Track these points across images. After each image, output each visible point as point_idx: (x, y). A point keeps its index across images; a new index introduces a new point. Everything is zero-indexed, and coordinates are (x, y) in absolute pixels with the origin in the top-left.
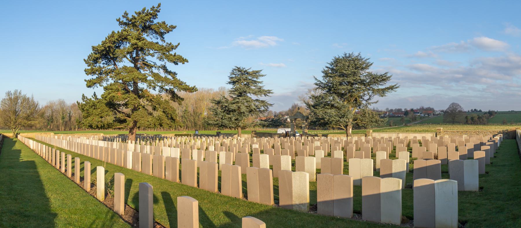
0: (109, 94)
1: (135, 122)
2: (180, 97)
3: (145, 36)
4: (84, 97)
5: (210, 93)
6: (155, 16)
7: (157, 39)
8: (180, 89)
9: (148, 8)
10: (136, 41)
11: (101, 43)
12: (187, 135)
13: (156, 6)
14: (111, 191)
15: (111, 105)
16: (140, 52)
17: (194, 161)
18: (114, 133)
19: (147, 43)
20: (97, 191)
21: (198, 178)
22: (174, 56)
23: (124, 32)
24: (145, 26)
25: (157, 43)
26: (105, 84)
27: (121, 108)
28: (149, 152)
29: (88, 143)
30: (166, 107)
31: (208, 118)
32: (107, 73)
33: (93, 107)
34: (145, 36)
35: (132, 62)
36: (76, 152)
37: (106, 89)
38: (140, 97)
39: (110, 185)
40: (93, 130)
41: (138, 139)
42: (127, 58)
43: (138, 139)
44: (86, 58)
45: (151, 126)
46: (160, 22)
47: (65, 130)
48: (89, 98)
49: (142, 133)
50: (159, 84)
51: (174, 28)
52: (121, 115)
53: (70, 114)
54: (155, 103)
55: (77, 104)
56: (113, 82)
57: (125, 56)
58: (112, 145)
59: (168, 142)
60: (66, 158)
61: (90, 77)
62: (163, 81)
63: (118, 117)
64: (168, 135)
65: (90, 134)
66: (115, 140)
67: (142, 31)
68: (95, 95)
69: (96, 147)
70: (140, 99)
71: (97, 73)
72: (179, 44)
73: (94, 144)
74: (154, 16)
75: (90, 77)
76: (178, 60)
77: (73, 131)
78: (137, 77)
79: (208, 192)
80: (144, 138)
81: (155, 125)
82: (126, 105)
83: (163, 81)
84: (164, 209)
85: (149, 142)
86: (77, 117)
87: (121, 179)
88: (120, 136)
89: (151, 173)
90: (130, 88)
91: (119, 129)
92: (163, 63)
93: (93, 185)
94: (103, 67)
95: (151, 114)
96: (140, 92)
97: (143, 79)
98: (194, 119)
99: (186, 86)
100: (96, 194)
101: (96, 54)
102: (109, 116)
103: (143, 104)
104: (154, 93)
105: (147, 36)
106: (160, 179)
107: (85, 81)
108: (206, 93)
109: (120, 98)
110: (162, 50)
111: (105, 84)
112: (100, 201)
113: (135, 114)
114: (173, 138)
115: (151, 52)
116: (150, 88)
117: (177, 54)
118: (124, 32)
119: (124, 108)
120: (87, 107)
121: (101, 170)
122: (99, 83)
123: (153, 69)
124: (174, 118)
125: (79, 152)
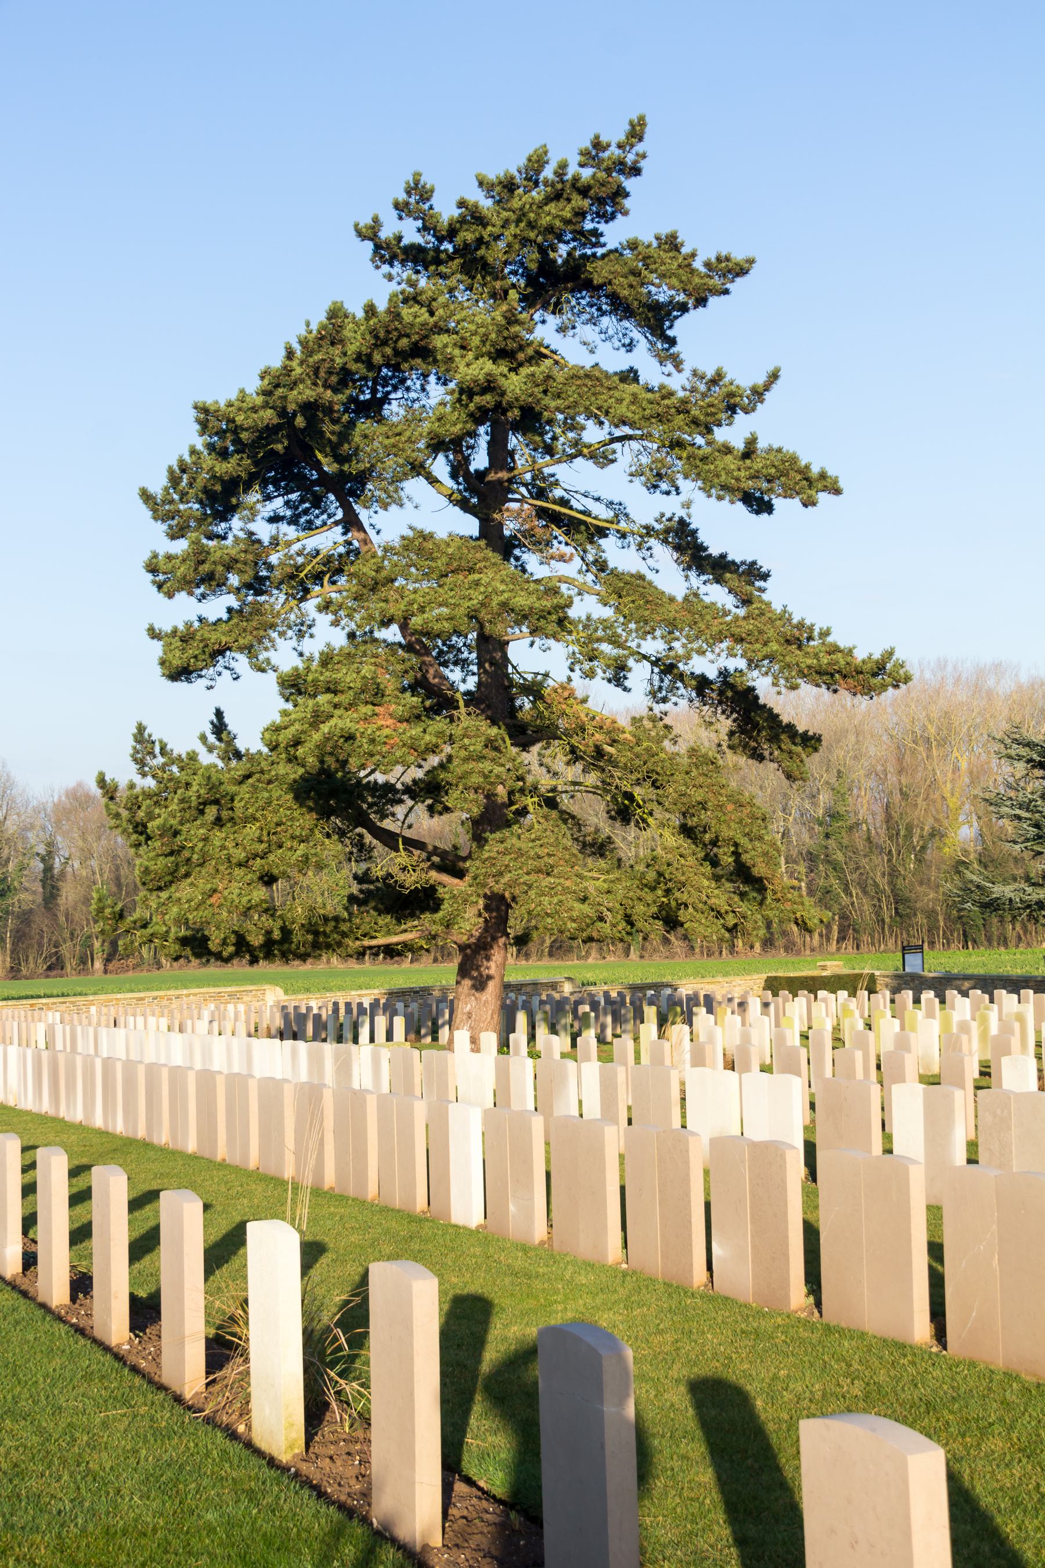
0: (318, 718)
1: (498, 907)
2: (790, 728)
3: (545, 329)
4: (144, 744)
5: (990, 694)
6: (609, 201)
7: (630, 347)
8: (795, 674)
9: (566, 152)
10: (489, 366)
11: (253, 385)
12: (849, 984)
13: (614, 134)
14: (350, 1388)
15: (335, 794)
16: (514, 441)
17: (905, 1162)
18: (362, 985)
19: (560, 376)
20: (254, 1390)
21: (937, 1282)
22: (748, 453)
23: (407, 312)
24: (546, 265)
25: (630, 376)
26: (285, 655)
27: (400, 810)
28: (593, 1110)
29: (178, 1060)
30: (698, 795)
31: (986, 860)
32: (299, 583)
33: (211, 812)
34: (545, 329)
35: (464, 505)
36: (99, 1122)
37: (293, 686)
38: (523, 735)
39: (336, 1346)
40: (214, 969)
41: (521, 1019)
42: (433, 481)
43: (521, 1019)
44: (158, 485)
45: (606, 928)
46: (647, 237)
47: (14, 973)
48: (180, 747)
49: (543, 977)
50: (653, 646)
51: (741, 270)
52: (402, 858)
53: (47, 859)
54: (627, 777)
55: (96, 791)
56: (338, 639)
57: (418, 469)
58: (344, 1068)
59: (717, 1030)
60: (29, 1167)
61: (184, 610)
62: (672, 626)
63: (378, 872)
64: (718, 987)
65: (191, 995)
66: (364, 1033)
67: (528, 301)
68: (220, 727)
69: (237, 1083)
70: (525, 746)
71: (234, 580)
72: (774, 376)
73: (218, 1064)
74: (601, 201)
75: (184, 610)
76: (765, 483)
77: (70, 980)
78: (504, 605)
79: (1010, 1376)
80: (560, 1014)
81: (629, 920)
82: (431, 791)
83: (672, 626)
84: (712, 1498)
85: (590, 1035)
86: (102, 886)
87: (410, 1312)
88: (396, 999)
89: (613, 1251)
90: (455, 675)
91: (391, 952)
92: (671, 506)
93: (224, 1348)
94: (275, 542)
95: (600, 848)
96: (525, 703)
97: (545, 614)
98: (893, 874)
99: (834, 649)
100: (245, 1412)
101: (224, 454)
102: (320, 867)
103: (546, 782)
104: (616, 703)
105: (562, 330)
106: (676, 1288)
107: (154, 634)
108: (962, 696)
109: (390, 746)
110: (659, 418)
111: (285, 655)
112: (272, 1462)
113: (491, 849)
114: (754, 1005)
115: (593, 434)
116: (590, 675)
117: (762, 444)
118: (407, 312)
119: (421, 809)
120: (171, 813)
121: (273, 1252)
122: (249, 650)
123: (609, 545)
124: (760, 869)
125: (119, 1127)
